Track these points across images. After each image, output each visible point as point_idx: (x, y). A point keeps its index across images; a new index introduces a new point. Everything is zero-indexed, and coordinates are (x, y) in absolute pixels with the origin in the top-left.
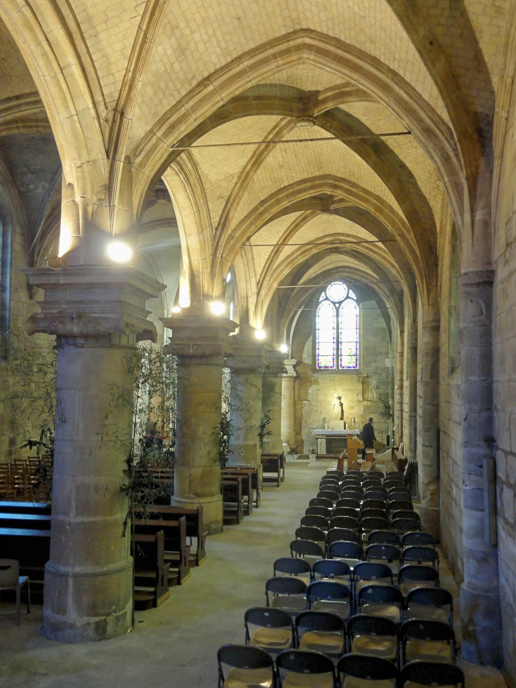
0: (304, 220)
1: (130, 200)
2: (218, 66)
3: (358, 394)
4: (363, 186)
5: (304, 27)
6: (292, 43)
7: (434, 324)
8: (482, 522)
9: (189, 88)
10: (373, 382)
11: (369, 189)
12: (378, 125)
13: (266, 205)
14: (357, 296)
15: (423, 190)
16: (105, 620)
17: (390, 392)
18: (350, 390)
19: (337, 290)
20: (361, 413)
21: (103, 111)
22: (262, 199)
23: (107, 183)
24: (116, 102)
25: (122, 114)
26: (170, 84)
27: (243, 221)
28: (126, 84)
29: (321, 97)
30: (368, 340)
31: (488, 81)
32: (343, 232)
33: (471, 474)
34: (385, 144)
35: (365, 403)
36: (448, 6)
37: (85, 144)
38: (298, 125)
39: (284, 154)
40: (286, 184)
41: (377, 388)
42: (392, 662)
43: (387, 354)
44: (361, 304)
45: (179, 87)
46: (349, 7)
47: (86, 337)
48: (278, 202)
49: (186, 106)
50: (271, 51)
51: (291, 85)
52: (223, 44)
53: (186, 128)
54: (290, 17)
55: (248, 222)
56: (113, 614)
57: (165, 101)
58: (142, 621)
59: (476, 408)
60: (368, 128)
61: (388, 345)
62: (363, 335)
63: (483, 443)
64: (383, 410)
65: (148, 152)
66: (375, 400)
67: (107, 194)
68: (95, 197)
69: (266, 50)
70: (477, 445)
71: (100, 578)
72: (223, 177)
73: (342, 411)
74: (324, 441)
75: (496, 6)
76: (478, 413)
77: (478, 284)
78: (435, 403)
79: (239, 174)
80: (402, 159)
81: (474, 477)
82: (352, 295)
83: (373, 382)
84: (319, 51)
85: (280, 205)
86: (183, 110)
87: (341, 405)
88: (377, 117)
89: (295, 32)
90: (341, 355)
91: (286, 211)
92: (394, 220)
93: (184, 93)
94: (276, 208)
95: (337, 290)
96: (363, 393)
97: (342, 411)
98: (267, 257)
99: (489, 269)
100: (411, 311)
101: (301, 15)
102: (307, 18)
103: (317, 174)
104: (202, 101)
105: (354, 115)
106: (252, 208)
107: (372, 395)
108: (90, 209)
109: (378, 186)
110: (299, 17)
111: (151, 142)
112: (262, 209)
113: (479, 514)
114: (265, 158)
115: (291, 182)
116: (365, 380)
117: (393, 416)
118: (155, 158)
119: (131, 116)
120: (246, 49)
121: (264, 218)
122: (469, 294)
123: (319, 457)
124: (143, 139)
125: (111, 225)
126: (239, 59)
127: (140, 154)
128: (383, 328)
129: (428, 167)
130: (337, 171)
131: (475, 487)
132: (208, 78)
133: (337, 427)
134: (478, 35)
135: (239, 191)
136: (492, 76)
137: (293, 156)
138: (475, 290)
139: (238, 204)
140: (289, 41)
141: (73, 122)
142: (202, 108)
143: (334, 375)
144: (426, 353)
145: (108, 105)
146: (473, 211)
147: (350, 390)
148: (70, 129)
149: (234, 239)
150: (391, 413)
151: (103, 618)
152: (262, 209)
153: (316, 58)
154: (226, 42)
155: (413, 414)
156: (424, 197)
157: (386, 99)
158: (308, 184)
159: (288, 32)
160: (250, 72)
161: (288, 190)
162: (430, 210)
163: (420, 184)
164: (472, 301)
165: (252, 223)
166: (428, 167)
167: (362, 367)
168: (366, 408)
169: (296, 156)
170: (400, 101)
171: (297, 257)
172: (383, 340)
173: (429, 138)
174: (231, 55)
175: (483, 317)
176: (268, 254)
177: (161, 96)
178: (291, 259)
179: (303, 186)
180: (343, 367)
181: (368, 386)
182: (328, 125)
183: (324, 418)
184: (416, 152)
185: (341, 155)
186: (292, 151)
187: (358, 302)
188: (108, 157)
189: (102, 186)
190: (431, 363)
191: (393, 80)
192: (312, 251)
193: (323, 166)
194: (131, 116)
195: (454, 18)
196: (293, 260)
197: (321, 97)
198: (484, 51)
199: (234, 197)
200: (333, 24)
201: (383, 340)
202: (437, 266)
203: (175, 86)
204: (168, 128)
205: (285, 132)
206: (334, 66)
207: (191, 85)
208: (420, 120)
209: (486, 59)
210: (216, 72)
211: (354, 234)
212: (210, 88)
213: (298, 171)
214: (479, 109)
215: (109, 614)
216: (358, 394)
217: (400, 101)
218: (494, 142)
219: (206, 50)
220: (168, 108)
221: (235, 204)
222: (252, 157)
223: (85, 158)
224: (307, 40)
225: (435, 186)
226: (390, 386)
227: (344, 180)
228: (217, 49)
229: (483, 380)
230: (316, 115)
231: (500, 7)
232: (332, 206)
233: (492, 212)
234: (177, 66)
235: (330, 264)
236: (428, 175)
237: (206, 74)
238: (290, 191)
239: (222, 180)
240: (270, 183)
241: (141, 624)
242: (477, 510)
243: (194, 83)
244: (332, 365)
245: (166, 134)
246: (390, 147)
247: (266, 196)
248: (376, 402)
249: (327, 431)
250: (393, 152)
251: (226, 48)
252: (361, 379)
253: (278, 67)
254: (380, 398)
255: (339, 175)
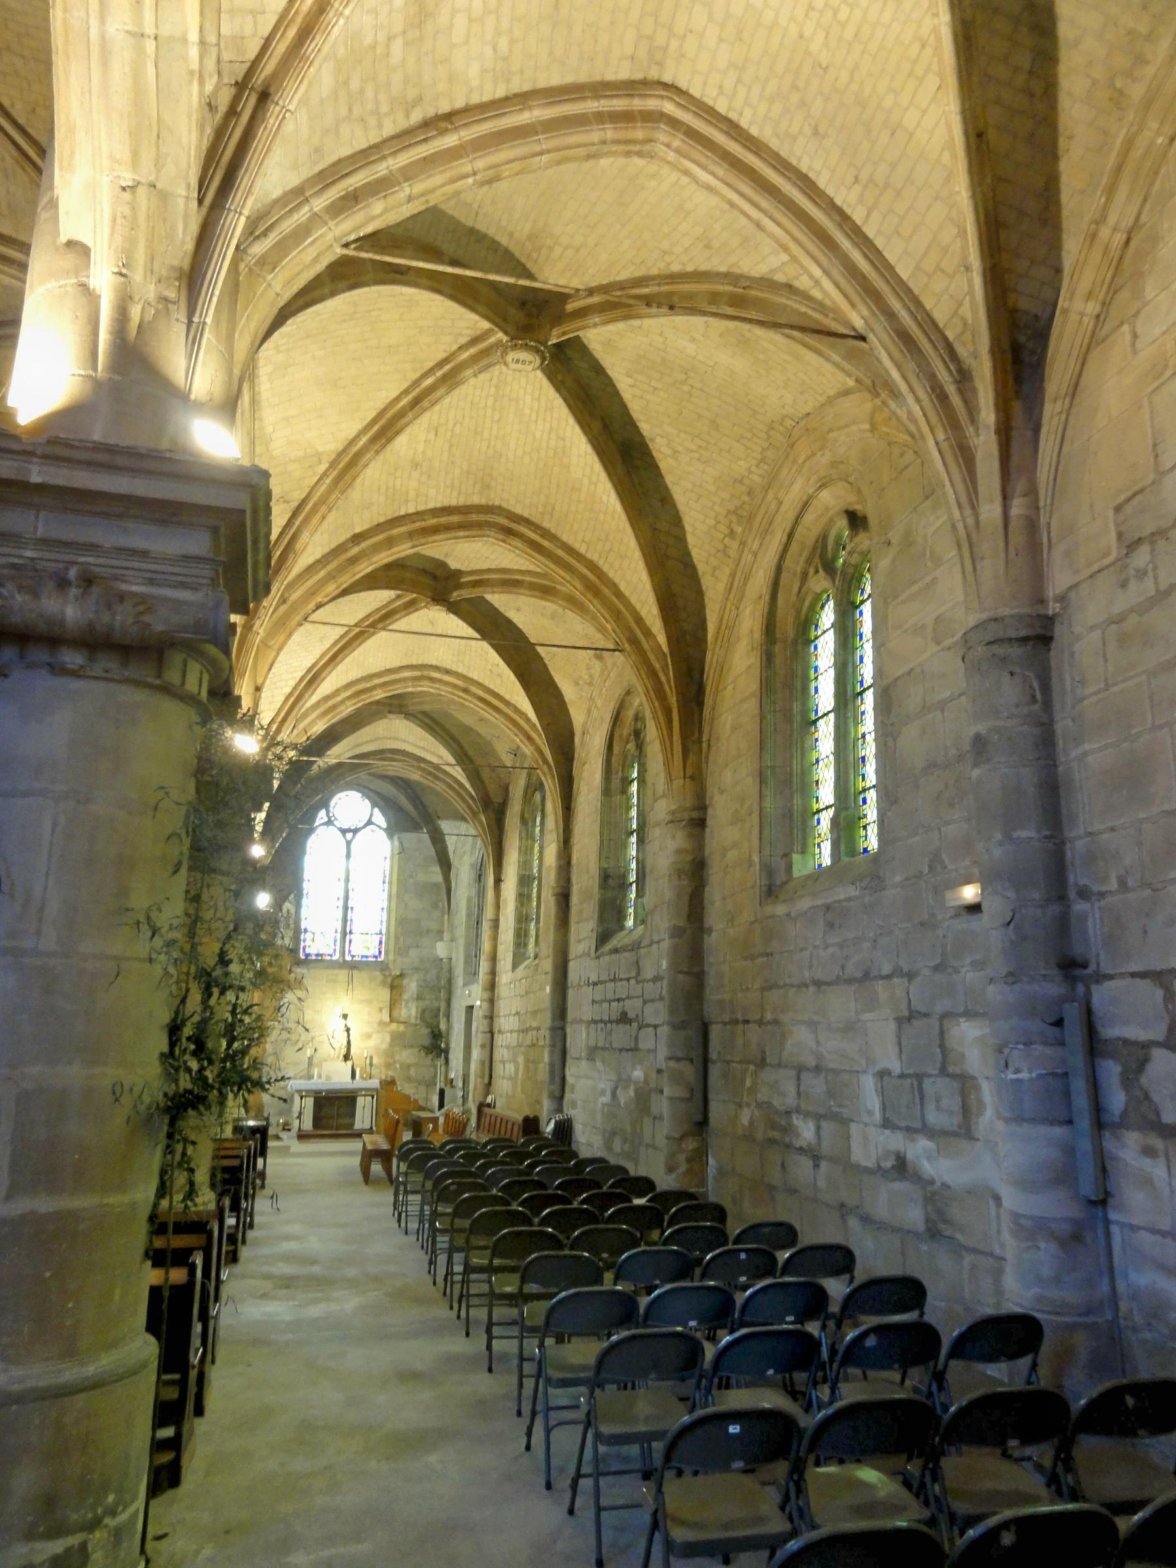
0: (382, 620)
1: (230, 338)
2: (475, 99)
3: (381, 1010)
4: (564, 538)
5: (667, 78)
6: (637, 104)
7: (695, 815)
8: (1070, 1151)
9: (402, 123)
10: (412, 986)
11: (577, 546)
12: (648, 401)
13: (363, 545)
14: (388, 821)
15: (695, 553)
16: (83, 1547)
17: (443, 1005)
18: (367, 1001)
19: (350, 806)
20: (385, 1046)
21: (211, 76)
22: (358, 530)
23: (186, 265)
24: (248, 65)
25: (264, 97)
26: (369, 94)
27: (310, 570)
28: (292, 20)
29: (570, 307)
30: (406, 905)
31: (1055, 245)
32: (439, 664)
33: (1031, 1043)
34: (647, 446)
35: (394, 1026)
36: (1027, 66)
37: (155, 134)
38: (511, 356)
39: (432, 436)
40: (411, 510)
41: (419, 997)
42: (925, 1529)
43: (440, 932)
44: (396, 838)
45: (384, 108)
46: (801, 37)
47: (96, 643)
48: (390, 542)
49: (390, 161)
50: (592, 106)
51: (523, 260)
52: (504, 42)
53: (385, 211)
54: (650, 38)
55: (322, 573)
56: (107, 1520)
57: (345, 130)
58: (165, 1536)
59: (1036, 896)
60: (625, 406)
61: (443, 916)
62: (398, 896)
63: (1056, 971)
64: (427, 1041)
65: (284, 238)
66: (413, 1021)
67: (184, 293)
68: (152, 287)
69: (584, 98)
70: (1044, 976)
71: (80, 1400)
72: (301, 453)
73: (349, 1042)
74: (309, 1102)
75: (1115, 89)
76: (1041, 906)
77: (1024, 640)
78: (695, 970)
79: (333, 457)
80: (670, 485)
81: (1038, 1049)
82: (379, 818)
83: (412, 986)
84: (691, 134)
85: (395, 550)
86: (381, 169)
87: (348, 1030)
88: (653, 383)
89: (645, 83)
90: (351, 933)
91: (371, 582)
92: (619, 612)
93: (389, 130)
94: (383, 555)
95: (350, 806)
96: (393, 1005)
97: (349, 1042)
98: (288, 690)
99: (1042, 612)
100: (561, 826)
101: (674, 44)
102: (683, 56)
103: (476, 500)
104: (428, 163)
105: (610, 372)
106: (333, 546)
107: (410, 1011)
108: (135, 312)
109: (599, 540)
110: (665, 49)
111: (296, 216)
112: (355, 550)
113: (1058, 1131)
114: (407, 425)
115: (421, 508)
116: (396, 983)
117: (446, 1051)
118: (303, 255)
119: (295, 101)
120: (542, 84)
121: (358, 569)
122: (1004, 659)
123: (302, 1136)
124: (276, 202)
125: (190, 371)
126: (522, 99)
127: (265, 234)
128: (435, 885)
129: (716, 508)
130: (517, 502)
131: (1044, 1072)
132: (449, 116)
133: (336, 1075)
134: (1062, 143)
135: (330, 491)
136: (1065, 236)
137: (446, 446)
138: (1015, 651)
139: (324, 518)
140: (632, 96)
141: (140, 52)
142: (429, 177)
143: (336, 971)
144: (679, 870)
145: (226, 68)
146: (1006, 497)
147: (367, 1001)
148: (127, 69)
149: (289, 603)
150: (443, 1045)
151: (73, 1540)
152: (355, 550)
153: (685, 148)
154: (512, 41)
155: (558, 1024)
156: (694, 567)
157: (825, 262)
158: (455, 519)
159: (633, 78)
160: (543, 133)
161: (414, 522)
162: (700, 593)
163: (690, 539)
164: (1012, 674)
165: (331, 577)
166: (716, 508)
167: (391, 957)
168: (396, 1038)
169: (451, 446)
170: (852, 270)
171: (342, 702)
172: (435, 906)
173: (909, 351)
174: (508, 81)
175: (1036, 707)
176: (293, 683)
177: (344, 111)
178: (330, 703)
179: (443, 520)
180: (353, 956)
181: (400, 995)
182: (560, 378)
183: (311, 1059)
184: (703, 472)
185: (541, 465)
186: (449, 434)
187: (390, 831)
188: (200, 201)
189: (173, 268)
190: (689, 890)
191: (841, 227)
192: (375, 693)
193: (493, 484)
194: (295, 101)
195: (1031, 95)
196: (334, 707)
197: (570, 307)
198: (1064, 179)
199: (315, 505)
200: (739, 81)
201: (435, 906)
202: (701, 704)
203: (377, 102)
204: (343, 198)
205: (468, 372)
206: (720, 172)
207: (407, 116)
208: (890, 315)
209: (1064, 198)
210: (467, 110)
211: (460, 671)
212: (450, 140)
213: (442, 484)
214: (1023, 304)
215: (94, 1524)
216: (381, 1010)
217: (852, 270)
218: (1047, 368)
219: (467, 42)
220: (345, 151)
221: (315, 520)
222: (374, 421)
223: (146, 174)
224: (669, 108)
225: (721, 547)
226: (443, 995)
227: (527, 522)
228: (488, 51)
229: (1046, 837)
230: (555, 341)
231: (1121, 92)
232: (455, 594)
233: (1041, 504)
234: (397, 47)
235: (372, 741)
236: (712, 522)
237: (445, 107)
238: (418, 525)
239: (294, 461)
240: (382, 499)
241: (163, 1545)
242: (1052, 1124)
243: (416, 117)
244: (331, 952)
245: (339, 208)
246: (655, 454)
247: (366, 526)
248: (416, 1025)
249: (319, 1082)
250: (657, 467)
251: (505, 59)
252: (389, 980)
253: (604, 142)
254: (423, 1019)
255: (518, 510)
